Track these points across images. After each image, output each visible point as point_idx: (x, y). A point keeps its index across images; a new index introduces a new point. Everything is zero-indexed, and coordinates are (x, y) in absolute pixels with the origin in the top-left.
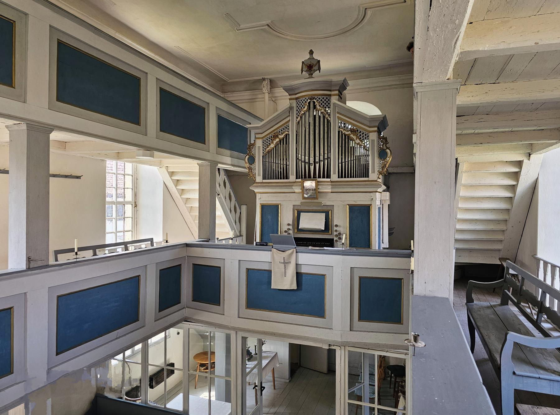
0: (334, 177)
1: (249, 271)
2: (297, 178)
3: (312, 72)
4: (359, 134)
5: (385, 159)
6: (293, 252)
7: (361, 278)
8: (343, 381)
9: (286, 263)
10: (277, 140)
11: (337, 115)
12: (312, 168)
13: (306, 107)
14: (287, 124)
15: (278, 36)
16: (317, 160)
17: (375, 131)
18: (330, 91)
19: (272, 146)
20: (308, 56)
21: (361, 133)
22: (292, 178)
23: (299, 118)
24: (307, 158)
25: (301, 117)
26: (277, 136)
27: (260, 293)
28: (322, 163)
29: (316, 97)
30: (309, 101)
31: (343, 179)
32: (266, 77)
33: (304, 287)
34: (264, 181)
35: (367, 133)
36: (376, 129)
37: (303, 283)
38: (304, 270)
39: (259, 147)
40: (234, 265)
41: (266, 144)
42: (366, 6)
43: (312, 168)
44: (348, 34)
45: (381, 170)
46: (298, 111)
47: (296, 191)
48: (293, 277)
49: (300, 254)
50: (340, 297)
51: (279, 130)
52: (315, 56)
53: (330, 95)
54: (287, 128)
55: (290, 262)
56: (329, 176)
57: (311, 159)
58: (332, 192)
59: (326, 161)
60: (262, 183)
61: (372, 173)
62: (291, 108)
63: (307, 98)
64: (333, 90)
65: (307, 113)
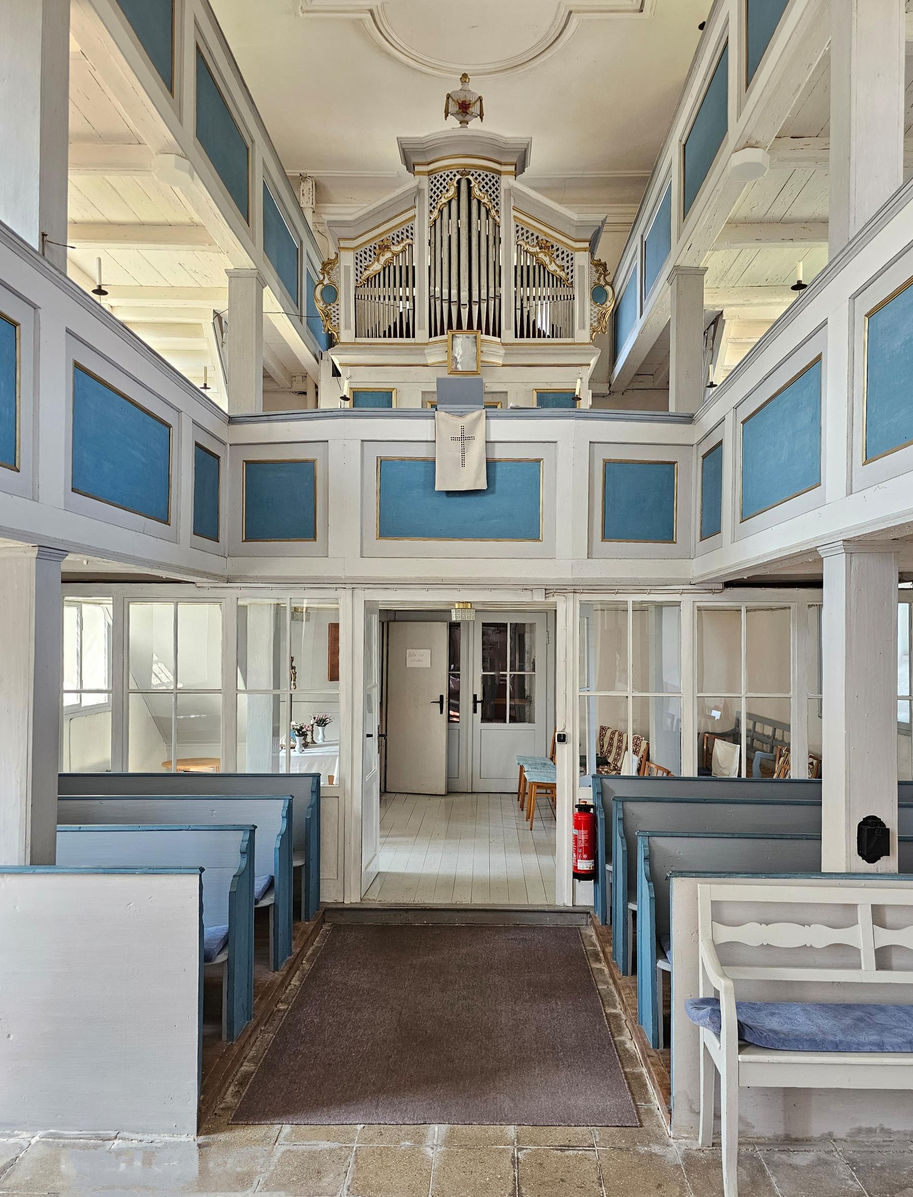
0: (508, 334)
1: (383, 463)
2: (430, 336)
3: (468, 117)
4: (556, 254)
6: (479, 417)
7: (606, 463)
8: (570, 656)
9: (464, 439)
10: (388, 255)
11: (514, 213)
13: (452, 191)
14: (410, 224)
16: (475, 298)
17: (585, 250)
18: (500, 163)
19: (377, 267)
20: (459, 86)
23: (436, 212)
24: (454, 292)
25: (441, 211)
26: (387, 247)
27: (409, 503)
29: (473, 171)
30: (458, 177)
31: (525, 340)
32: (309, 172)
33: (498, 486)
34: (359, 340)
35: (570, 252)
36: (586, 245)
38: (500, 453)
39: (347, 268)
40: (345, 451)
41: (360, 267)
42: (571, 9)
44: (521, 70)
45: (595, 324)
47: (431, 360)
50: (569, 500)
51: (391, 234)
53: (499, 173)
56: (497, 333)
58: (503, 366)
59: (492, 303)
60: (355, 343)
62: (419, 191)
63: (455, 172)
64: (506, 164)
65: (454, 204)
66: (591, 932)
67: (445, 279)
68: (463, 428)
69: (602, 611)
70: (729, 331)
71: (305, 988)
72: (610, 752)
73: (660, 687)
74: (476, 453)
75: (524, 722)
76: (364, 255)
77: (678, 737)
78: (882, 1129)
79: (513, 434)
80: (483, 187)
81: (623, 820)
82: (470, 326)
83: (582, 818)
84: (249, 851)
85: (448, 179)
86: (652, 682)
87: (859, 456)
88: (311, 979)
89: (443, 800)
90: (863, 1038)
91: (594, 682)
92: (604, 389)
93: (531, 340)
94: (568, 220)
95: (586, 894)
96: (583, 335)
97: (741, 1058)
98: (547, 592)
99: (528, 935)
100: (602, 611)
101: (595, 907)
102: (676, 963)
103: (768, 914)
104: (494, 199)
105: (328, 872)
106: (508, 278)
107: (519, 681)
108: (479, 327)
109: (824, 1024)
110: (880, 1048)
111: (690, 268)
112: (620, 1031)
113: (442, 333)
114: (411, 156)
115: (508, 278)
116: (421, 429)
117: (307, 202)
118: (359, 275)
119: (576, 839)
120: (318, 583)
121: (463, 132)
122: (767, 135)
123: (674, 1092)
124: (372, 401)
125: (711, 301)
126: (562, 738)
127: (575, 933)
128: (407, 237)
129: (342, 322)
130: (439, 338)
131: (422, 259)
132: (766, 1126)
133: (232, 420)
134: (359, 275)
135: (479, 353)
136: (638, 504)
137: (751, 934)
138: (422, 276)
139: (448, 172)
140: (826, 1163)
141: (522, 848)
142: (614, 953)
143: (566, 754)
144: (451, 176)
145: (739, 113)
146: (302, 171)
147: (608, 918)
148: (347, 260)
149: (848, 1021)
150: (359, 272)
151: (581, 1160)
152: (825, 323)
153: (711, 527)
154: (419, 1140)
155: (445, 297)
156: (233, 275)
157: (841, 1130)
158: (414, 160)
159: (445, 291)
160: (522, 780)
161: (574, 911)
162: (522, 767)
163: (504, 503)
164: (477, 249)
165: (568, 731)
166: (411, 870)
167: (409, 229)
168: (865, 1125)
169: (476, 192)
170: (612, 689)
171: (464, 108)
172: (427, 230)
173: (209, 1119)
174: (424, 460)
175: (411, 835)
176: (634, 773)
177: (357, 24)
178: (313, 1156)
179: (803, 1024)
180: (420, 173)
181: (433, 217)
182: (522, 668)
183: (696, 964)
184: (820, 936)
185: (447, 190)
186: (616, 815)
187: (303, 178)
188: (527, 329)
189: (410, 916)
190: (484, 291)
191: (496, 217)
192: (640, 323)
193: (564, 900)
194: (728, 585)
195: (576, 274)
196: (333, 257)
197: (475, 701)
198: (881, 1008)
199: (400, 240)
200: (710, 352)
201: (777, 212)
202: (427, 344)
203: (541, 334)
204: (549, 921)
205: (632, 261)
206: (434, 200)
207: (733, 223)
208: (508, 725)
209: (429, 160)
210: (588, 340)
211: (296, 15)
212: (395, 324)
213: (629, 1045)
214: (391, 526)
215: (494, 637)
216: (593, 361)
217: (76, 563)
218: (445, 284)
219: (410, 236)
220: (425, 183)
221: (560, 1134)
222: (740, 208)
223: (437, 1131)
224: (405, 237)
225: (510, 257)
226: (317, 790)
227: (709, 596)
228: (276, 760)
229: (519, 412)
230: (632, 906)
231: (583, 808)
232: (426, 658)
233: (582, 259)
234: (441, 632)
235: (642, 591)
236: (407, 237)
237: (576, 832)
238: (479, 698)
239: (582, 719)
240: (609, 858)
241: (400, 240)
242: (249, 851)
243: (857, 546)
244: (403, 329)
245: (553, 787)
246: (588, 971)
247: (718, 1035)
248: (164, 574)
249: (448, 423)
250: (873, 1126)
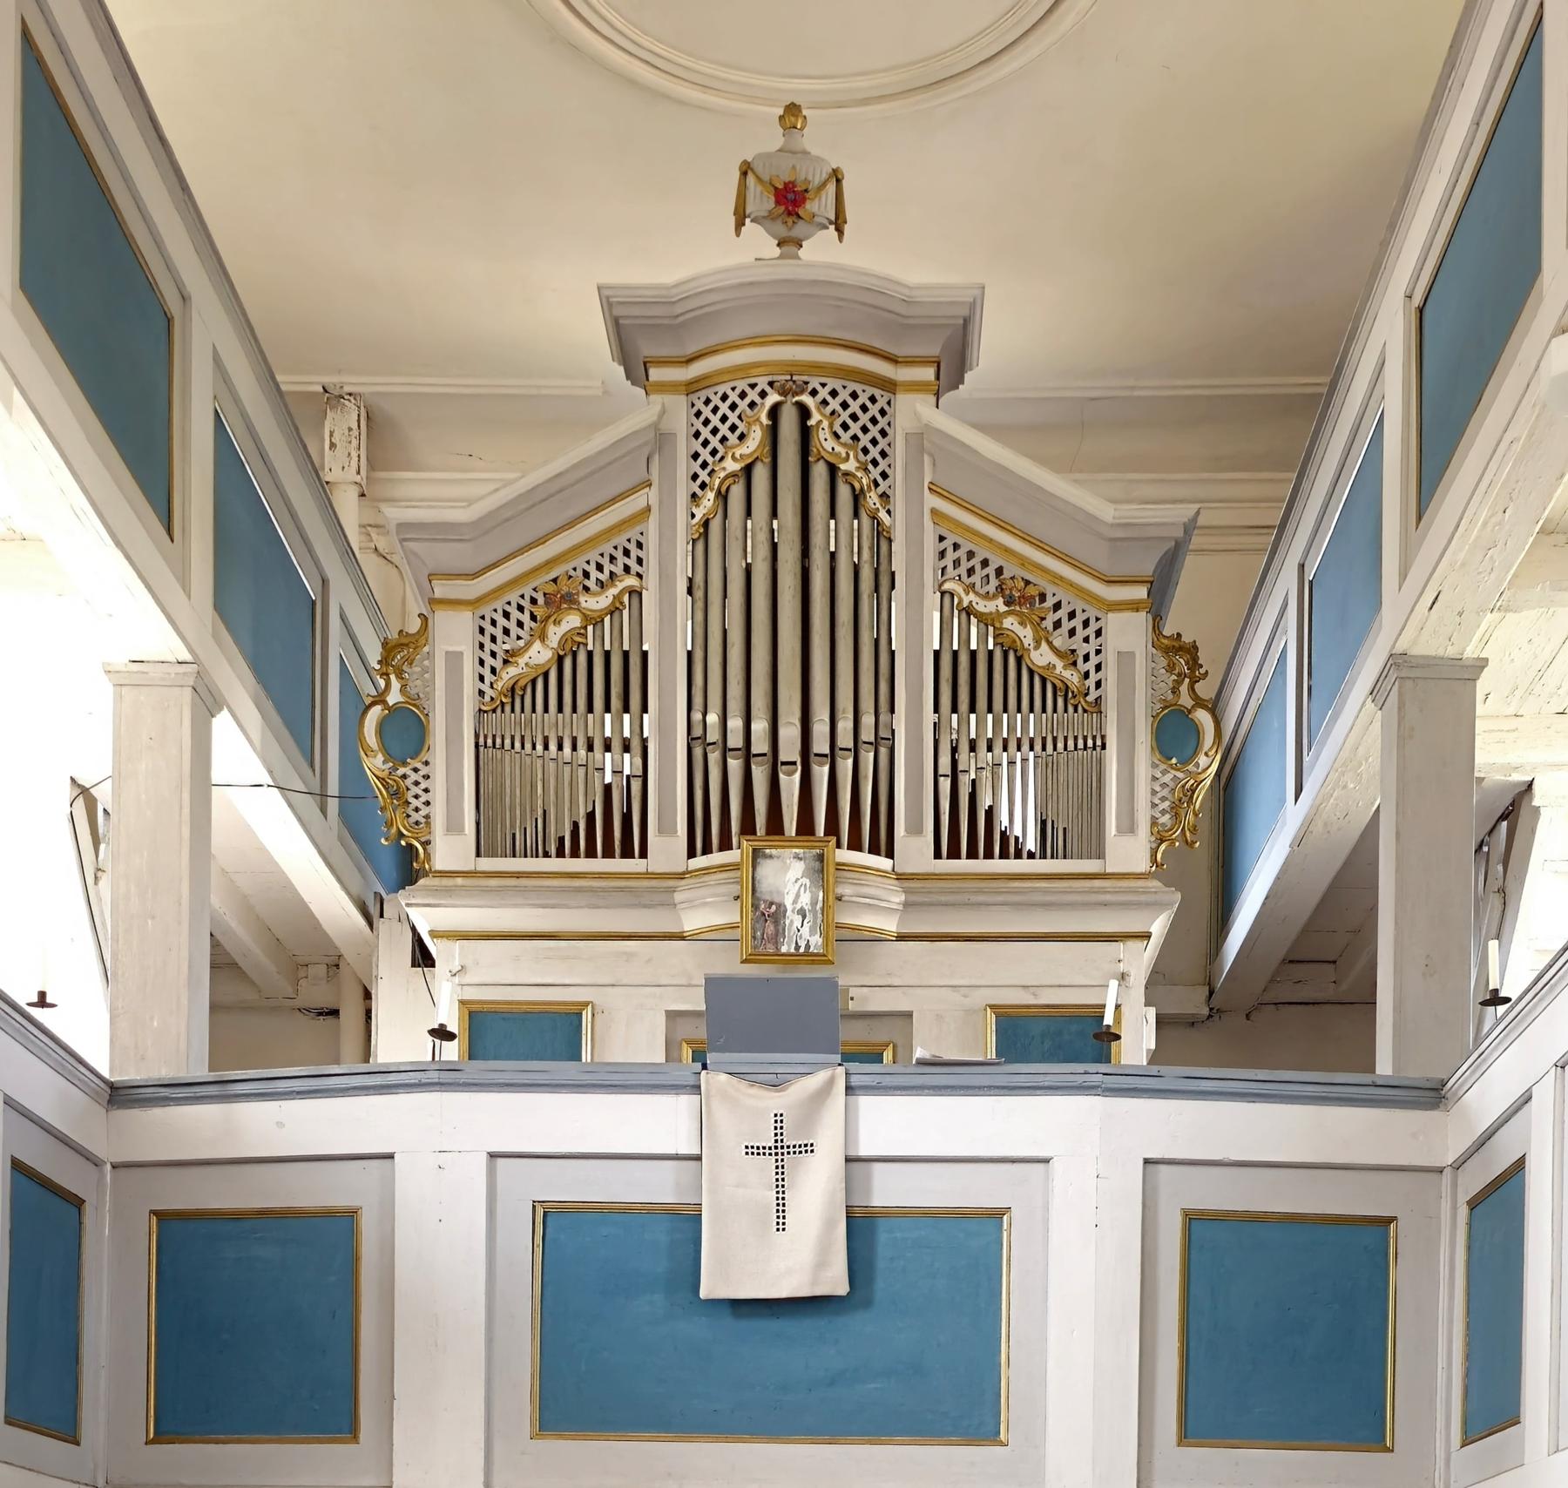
0: (915, 850)
1: (553, 1219)
2: (691, 854)
3: (800, 229)
5: (1185, 762)
9: (783, 1151)
10: (572, 621)
11: (932, 501)
12: (791, 784)
13: (756, 438)
14: (633, 534)
16: (821, 745)
17: (1134, 606)
19: (539, 654)
20: (773, 139)
21: (1062, 613)
24: (760, 726)
25: (723, 497)
28: (846, 766)
29: (814, 383)
30: (773, 398)
31: (963, 865)
33: (882, 1286)
34: (486, 864)
35: (1092, 613)
36: (1141, 592)
37: (881, 1264)
38: (889, 1189)
39: (454, 659)
43: (791, 784)
47: (692, 921)
48: (829, 1224)
49: (865, 1102)
53: (890, 386)
54: (632, 556)
55: (809, 1148)
56: (883, 844)
57: (783, 732)
58: (902, 938)
59: (868, 757)
61: (1120, 831)
62: (661, 440)
63: (762, 383)
65: (761, 475)
68: (779, 1119)
74: (817, 1190)
76: (501, 621)
79: (932, 1140)
80: (845, 427)
85: (743, 405)
92: (1193, 1002)
93: (981, 865)
94: (1086, 522)
96: (1129, 851)
104: (875, 463)
106: (914, 686)
111: (1429, 663)
113: (725, 845)
114: (642, 337)
115: (914, 686)
116: (660, 1122)
118: (488, 677)
121: (787, 270)
124: (522, 1041)
125: (1498, 755)
128: (627, 569)
130: (717, 858)
131: (667, 631)
133: (118, 1095)
134: (488, 677)
139: (742, 385)
144: (753, 395)
146: (327, 379)
148: (455, 635)
155: (735, 740)
156: (132, 679)
158: (647, 349)
167: (632, 547)
169: (824, 441)
171: (788, 203)
172: (682, 548)
181: (700, 513)
185: (742, 437)
187: (332, 398)
188: (968, 831)
190: (845, 725)
191: (883, 515)
192: (1293, 816)
195: (1110, 675)
196: (414, 626)
199: (604, 577)
200: (1496, 900)
202: (681, 876)
203: (1009, 848)
206: (704, 465)
209: (692, 349)
210: (1143, 865)
212: (591, 817)
216: (1159, 927)
219: (635, 567)
224: (619, 570)
225: (919, 627)
229: (944, 1077)
233: (1127, 634)
236: (627, 569)
241: (604, 577)
244: (615, 830)
249: (739, 1106)
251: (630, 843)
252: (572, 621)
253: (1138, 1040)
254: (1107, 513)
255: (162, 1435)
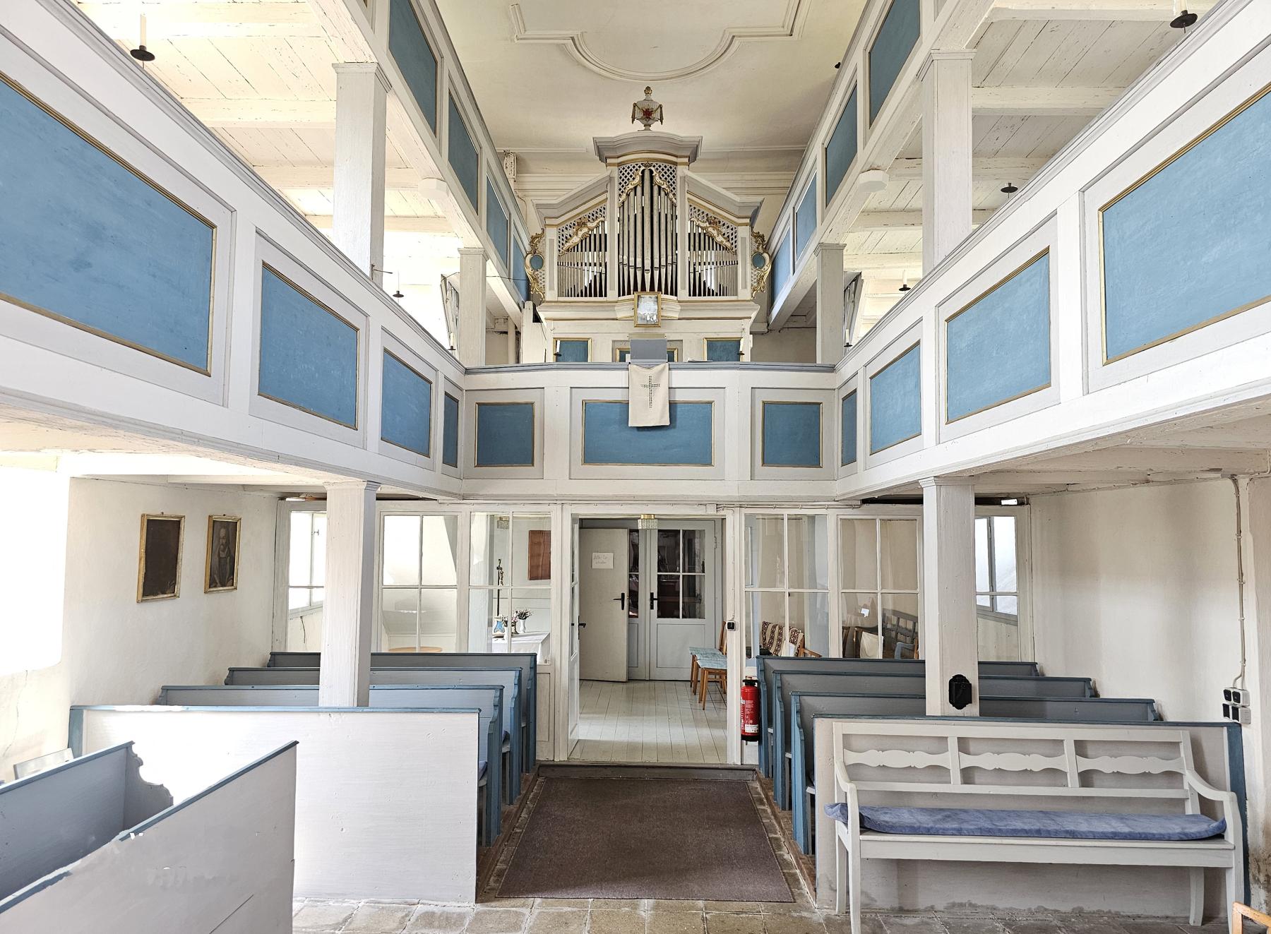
0: (683, 293)
1: (586, 404)
2: (538, 207)
9: (652, 386)
10: (585, 230)
12: (648, 276)
13: (638, 179)
15: (579, 64)
16: (656, 265)
19: (576, 240)
20: (643, 97)
22: (612, 293)
24: (639, 260)
25: (628, 195)
27: (608, 436)
28: (663, 271)
32: (512, 149)
38: (680, 396)
39: (551, 241)
40: (558, 398)
42: (735, 32)
43: (648, 276)
46: (622, 185)
50: (735, 433)
52: (653, 97)
53: (676, 164)
56: (674, 292)
59: (670, 268)
62: (611, 179)
65: (639, 189)
66: (757, 785)
67: (632, 249)
69: (765, 522)
70: (867, 288)
71: (540, 812)
72: (771, 644)
73: (814, 584)
75: (694, 617)
77: (826, 628)
78: (970, 904)
79: (692, 382)
81: (781, 688)
82: (652, 289)
83: (748, 690)
84: (499, 706)
86: (806, 581)
87: (944, 419)
88: (535, 814)
89: (625, 686)
90: (947, 826)
91: (757, 582)
92: (763, 328)
93: (702, 298)
94: (732, 202)
95: (752, 753)
96: (745, 293)
97: (862, 837)
98: (718, 507)
99: (705, 787)
100: (765, 522)
101: (759, 766)
102: (819, 790)
103: (885, 742)
105: (542, 735)
106: (683, 242)
107: (690, 582)
108: (660, 289)
109: (925, 820)
110: (959, 832)
111: (829, 245)
112: (780, 848)
113: (629, 293)
114: (604, 151)
115: (683, 242)
116: (616, 378)
117: (510, 174)
119: (743, 707)
120: (535, 499)
121: (647, 133)
122: (887, 161)
123: (818, 876)
124: (572, 352)
125: (851, 265)
126: (732, 626)
127: (744, 785)
129: (547, 285)
130: (627, 297)
131: (611, 228)
132: (884, 898)
133: (468, 371)
135: (660, 310)
136: (792, 436)
137: (872, 758)
138: (612, 243)
140: (927, 924)
141: (697, 723)
142: (775, 798)
143: (734, 642)
145: (865, 144)
147: (770, 772)
148: (552, 234)
149: (940, 817)
150: (561, 245)
151: (751, 919)
152: (921, 319)
153: (849, 457)
154: (635, 907)
155: (632, 263)
156: (464, 253)
157: (940, 905)
158: (606, 154)
159: (632, 259)
160: (696, 667)
161: (741, 769)
162: (694, 657)
163: (685, 436)
164: (655, 226)
165: (737, 620)
166: (605, 738)
168: (958, 901)
169: (657, 179)
170: (775, 587)
171: (647, 114)
172: (617, 209)
173: (483, 893)
174: (619, 402)
175: (601, 713)
176: (792, 655)
177: (562, 48)
178: (560, 915)
179: (906, 818)
180: (611, 165)
182: (692, 569)
183: (834, 783)
184: (921, 759)
186: (776, 684)
187: (507, 154)
188: (698, 288)
189: (608, 772)
190: (663, 260)
192: (792, 279)
193: (734, 759)
194: (865, 501)
195: (739, 244)
196: (540, 232)
197: (652, 599)
198: (965, 811)
201: (901, 204)
203: (710, 293)
204: (721, 776)
205: (784, 227)
207: (867, 212)
208: (681, 620)
210: (749, 298)
211: (512, 40)
213: (786, 856)
214: (594, 454)
215: (668, 542)
216: (753, 315)
217: (385, 490)
218: (632, 254)
220: (615, 172)
221: (736, 906)
222: (873, 201)
223: (646, 905)
225: (684, 227)
226: (534, 666)
227: (850, 511)
228: (490, 645)
229: (695, 365)
230: (788, 755)
231: (749, 683)
232: (611, 559)
233: (744, 232)
234: (622, 537)
235: (795, 507)
237: (743, 702)
238: (655, 596)
239: (748, 615)
240: (770, 723)
242: (499, 706)
243: (943, 480)
244: (597, 289)
245: (724, 672)
246: (755, 811)
247: (846, 824)
248: (421, 495)
249: (638, 374)
250: (964, 901)
251: (602, 292)
252: (585, 230)
253: (746, 345)
254: (737, 199)
255: (478, 465)
